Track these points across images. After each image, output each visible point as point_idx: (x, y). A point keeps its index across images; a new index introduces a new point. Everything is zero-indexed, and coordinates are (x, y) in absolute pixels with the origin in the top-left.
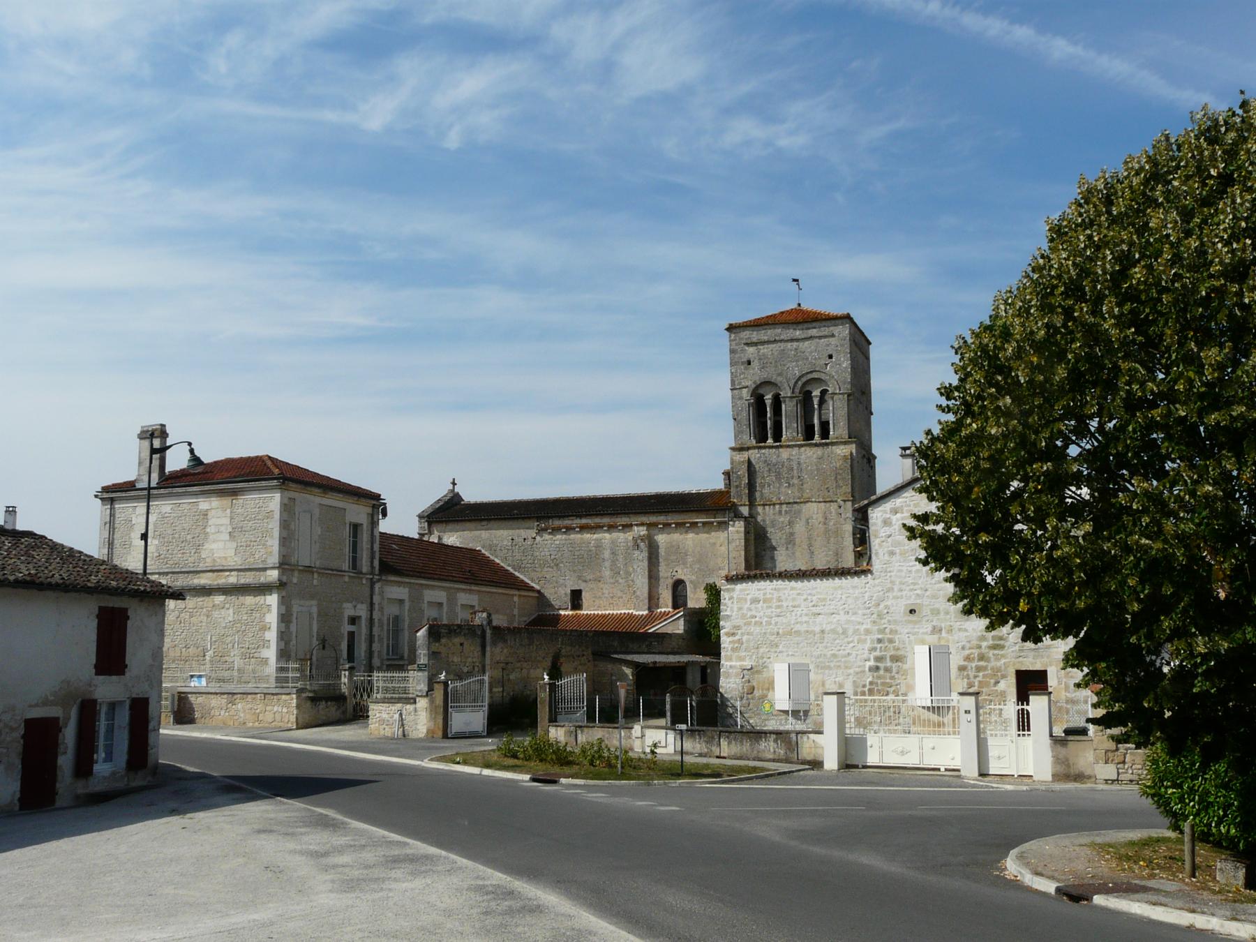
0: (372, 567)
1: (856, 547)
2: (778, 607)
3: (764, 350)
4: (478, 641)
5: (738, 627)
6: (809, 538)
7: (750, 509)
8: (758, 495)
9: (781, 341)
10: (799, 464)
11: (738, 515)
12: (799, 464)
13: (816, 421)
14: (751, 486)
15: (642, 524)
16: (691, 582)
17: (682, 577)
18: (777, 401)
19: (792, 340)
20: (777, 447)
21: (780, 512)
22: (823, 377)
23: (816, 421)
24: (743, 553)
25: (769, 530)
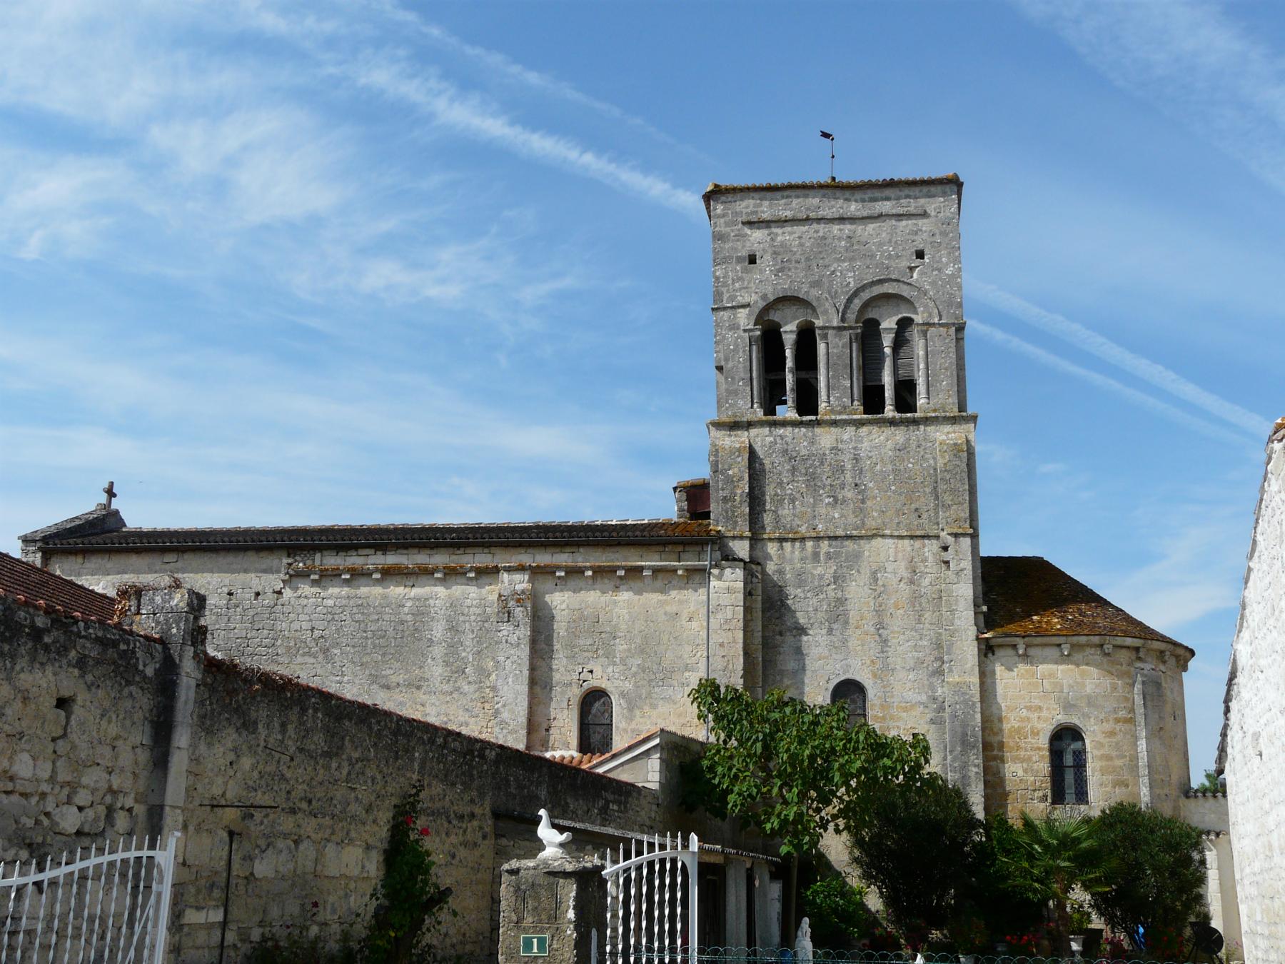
1: (980, 631)
3: (785, 235)
4: (145, 701)
6: (879, 612)
7: (751, 547)
8: (767, 519)
9: (819, 220)
10: (857, 459)
11: (729, 558)
12: (857, 459)
13: (887, 379)
14: (755, 500)
15: (521, 568)
16: (623, 695)
17: (604, 684)
18: (807, 338)
19: (842, 220)
20: (809, 424)
21: (816, 555)
22: (905, 291)
23: (887, 379)
24: (740, 635)
25: (791, 591)
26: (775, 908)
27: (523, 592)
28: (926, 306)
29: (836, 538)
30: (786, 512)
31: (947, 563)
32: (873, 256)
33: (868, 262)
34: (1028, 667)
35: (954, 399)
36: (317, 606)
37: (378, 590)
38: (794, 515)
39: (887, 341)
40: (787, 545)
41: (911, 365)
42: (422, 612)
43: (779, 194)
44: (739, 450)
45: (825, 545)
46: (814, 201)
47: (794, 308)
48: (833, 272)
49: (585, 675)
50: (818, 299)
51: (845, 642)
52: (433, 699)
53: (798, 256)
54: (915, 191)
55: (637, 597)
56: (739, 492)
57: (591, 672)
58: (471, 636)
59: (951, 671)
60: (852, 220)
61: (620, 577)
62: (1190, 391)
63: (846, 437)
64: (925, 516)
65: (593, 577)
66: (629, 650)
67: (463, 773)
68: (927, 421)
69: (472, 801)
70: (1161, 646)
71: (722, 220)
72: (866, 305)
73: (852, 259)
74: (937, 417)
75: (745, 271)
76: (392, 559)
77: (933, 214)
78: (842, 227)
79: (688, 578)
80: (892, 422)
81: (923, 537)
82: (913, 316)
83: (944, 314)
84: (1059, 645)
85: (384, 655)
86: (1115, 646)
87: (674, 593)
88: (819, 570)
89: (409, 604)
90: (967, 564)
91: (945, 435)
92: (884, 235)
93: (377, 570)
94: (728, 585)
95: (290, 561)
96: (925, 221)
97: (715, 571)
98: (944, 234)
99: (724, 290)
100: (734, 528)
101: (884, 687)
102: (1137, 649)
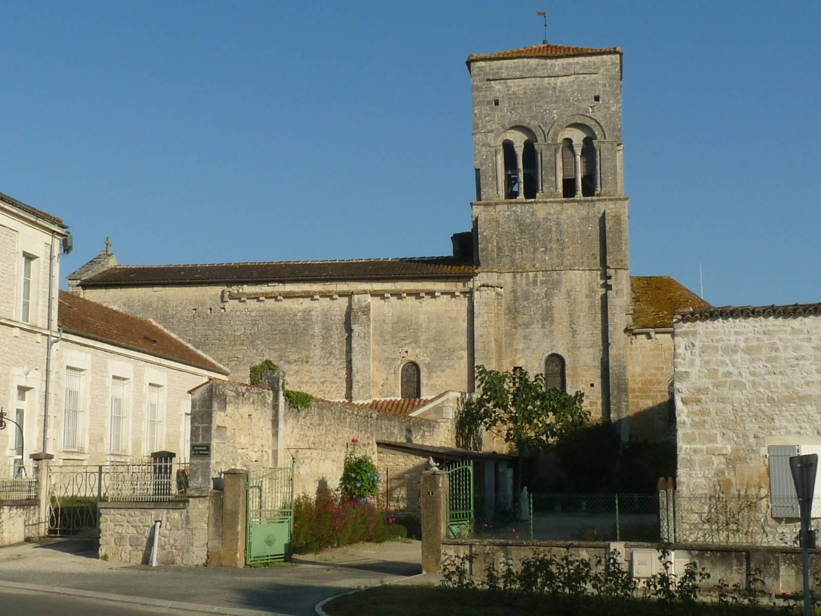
0: (49, 320)
2: (769, 360)
5: (705, 391)
10: (558, 224)
26: (510, 483)
38: (522, 258)
42: (307, 316)
51: (551, 332)
57: (407, 352)
58: (336, 332)
67: (364, 426)
69: (368, 438)
75: (492, 109)
80: (579, 202)
89: (300, 314)
99: (480, 122)
100: (487, 267)
101: (574, 357)
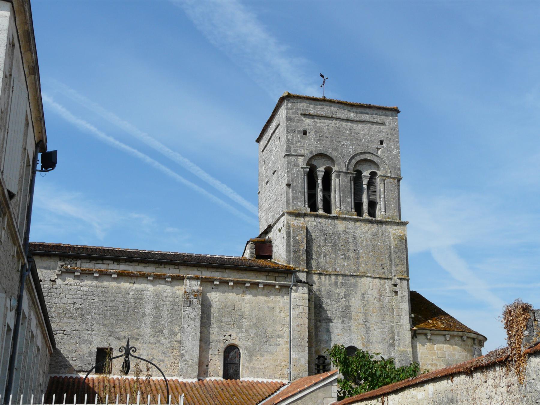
3: (321, 124)
6: (365, 314)
8: (313, 263)
9: (337, 119)
10: (355, 237)
13: (365, 200)
15: (197, 278)
17: (237, 342)
18: (328, 174)
19: (347, 120)
21: (336, 283)
22: (375, 159)
23: (365, 200)
25: (324, 300)
27: (198, 291)
28: (384, 168)
29: (345, 275)
30: (322, 260)
31: (396, 292)
32: (361, 140)
33: (359, 143)
34: (431, 345)
35: (397, 214)
36: (78, 290)
37: (114, 284)
39: (365, 182)
40: (323, 277)
41: (375, 195)
42: (139, 298)
43: (318, 103)
44: (301, 227)
45: (340, 278)
46: (334, 109)
47: (323, 160)
48: (343, 145)
49: (227, 337)
50: (336, 157)
51: (350, 327)
52: (145, 346)
53: (327, 135)
54: (380, 112)
55: (254, 298)
56: (301, 248)
58: (167, 313)
59: (399, 345)
60: (352, 121)
61: (247, 287)
62: (238, 198)
63: (350, 226)
64: (385, 268)
65: (263, 288)
66: (250, 325)
68: (336, 218)
70: (473, 335)
71: (291, 111)
72: (358, 163)
73: (351, 140)
74: (391, 222)
75: (302, 138)
76: (123, 267)
77: (387, 124)
78: (347, 124)
79: (263, 288)
81: (385, 279)
82: (377, 171)
83: (393, 172)
84: (445, 335)
85: (117, 320)
86: (468, 337)
87: (272, 297)
88: (338, 291)
89: (132, 293)
90: (406, 294)
91: (393, 230)
92: (366, 131)
93: (115, 273)
94: (300, 295)
95: (63, 263)
96: (384, 127)
97: (294, 288)
98: (392, 134)
100: (299, 267)
102: (462, 337)
